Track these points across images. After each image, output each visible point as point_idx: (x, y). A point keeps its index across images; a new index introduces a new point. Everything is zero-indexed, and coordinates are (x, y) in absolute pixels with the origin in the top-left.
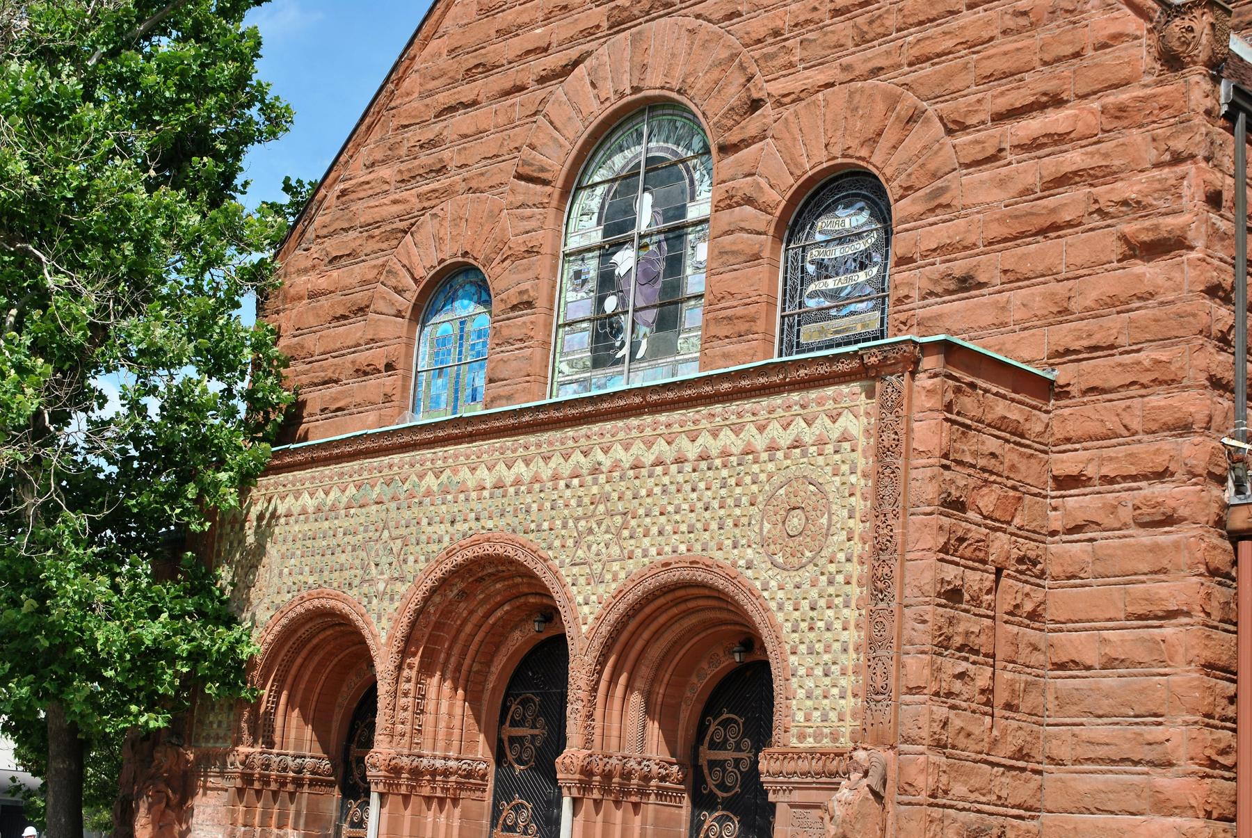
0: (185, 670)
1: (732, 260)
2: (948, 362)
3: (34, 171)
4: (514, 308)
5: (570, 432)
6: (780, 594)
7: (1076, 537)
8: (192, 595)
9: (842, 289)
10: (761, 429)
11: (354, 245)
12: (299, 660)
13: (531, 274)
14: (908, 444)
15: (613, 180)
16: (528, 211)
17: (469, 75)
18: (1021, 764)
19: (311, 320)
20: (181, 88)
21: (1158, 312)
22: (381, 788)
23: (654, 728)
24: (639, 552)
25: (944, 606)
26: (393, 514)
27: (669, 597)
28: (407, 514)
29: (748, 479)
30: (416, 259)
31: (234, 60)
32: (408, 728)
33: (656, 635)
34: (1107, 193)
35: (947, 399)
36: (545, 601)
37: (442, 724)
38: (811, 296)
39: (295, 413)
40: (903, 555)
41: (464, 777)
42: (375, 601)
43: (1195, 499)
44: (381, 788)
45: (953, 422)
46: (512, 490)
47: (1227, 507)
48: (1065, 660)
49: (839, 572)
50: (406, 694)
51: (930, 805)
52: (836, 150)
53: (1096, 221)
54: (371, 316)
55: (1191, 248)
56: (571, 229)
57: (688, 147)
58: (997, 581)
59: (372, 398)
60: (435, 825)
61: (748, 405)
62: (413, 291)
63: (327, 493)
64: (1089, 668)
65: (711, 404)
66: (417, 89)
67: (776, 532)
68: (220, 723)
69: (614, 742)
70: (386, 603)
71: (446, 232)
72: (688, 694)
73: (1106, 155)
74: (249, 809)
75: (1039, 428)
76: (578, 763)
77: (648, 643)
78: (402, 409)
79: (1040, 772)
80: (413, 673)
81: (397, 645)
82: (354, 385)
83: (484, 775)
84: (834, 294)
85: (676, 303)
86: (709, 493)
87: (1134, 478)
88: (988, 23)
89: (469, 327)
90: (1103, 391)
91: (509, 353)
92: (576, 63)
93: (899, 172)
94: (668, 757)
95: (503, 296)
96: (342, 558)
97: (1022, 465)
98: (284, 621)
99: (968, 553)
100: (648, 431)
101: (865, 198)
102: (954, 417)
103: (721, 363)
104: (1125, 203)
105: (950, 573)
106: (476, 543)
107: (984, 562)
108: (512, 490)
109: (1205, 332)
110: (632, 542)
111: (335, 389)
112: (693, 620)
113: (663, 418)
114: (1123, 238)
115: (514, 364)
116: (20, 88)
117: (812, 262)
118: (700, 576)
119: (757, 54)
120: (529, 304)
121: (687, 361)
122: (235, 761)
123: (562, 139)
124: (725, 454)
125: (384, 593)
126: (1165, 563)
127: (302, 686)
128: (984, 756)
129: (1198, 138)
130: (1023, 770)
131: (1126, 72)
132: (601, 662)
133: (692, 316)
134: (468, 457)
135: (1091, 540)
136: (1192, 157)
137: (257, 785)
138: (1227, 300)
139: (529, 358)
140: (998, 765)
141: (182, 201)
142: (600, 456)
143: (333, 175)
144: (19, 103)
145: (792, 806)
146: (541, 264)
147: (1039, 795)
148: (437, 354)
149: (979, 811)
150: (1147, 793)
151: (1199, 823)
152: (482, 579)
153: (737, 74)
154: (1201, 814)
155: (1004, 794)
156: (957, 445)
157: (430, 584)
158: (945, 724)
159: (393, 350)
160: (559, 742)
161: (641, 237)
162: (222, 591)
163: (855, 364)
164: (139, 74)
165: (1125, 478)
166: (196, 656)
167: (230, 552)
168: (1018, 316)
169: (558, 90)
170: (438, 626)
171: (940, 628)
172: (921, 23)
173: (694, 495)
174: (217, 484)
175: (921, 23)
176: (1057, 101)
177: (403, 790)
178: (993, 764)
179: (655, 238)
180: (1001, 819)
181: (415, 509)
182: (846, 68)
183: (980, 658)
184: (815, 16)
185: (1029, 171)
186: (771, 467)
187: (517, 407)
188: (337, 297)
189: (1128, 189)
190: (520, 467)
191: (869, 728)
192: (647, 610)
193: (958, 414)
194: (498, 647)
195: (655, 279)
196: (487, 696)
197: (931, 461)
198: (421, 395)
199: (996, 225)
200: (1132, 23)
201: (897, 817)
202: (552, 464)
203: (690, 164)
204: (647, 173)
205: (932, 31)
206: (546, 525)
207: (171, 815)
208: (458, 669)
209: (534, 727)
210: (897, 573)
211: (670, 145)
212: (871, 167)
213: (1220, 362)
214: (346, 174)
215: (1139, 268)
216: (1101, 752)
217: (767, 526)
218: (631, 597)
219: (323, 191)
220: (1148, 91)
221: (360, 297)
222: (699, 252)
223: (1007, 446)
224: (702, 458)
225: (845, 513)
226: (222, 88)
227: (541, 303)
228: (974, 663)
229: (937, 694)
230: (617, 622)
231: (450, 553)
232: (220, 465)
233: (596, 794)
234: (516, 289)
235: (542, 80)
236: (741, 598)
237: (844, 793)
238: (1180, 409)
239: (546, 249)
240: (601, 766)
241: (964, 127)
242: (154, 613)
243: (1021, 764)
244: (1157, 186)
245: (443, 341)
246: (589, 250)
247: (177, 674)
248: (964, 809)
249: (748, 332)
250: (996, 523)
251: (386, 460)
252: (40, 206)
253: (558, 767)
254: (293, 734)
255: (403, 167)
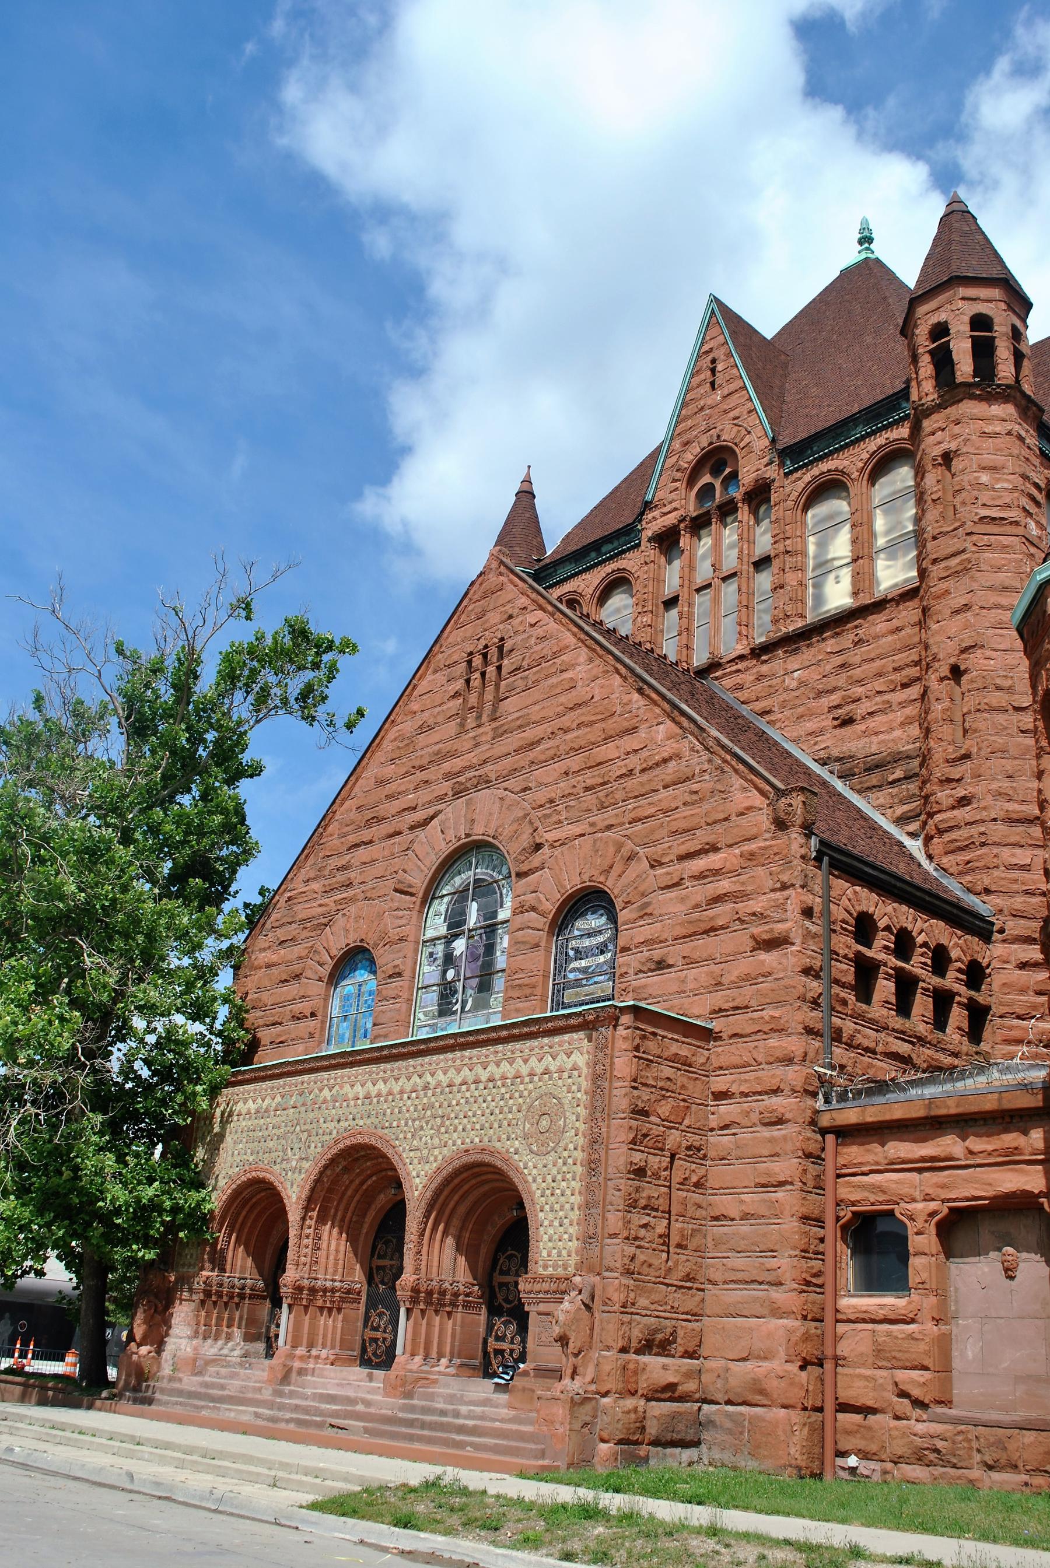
0: (168, 1219)
1: (522, 947)
2: (636, 1019)
3: (81, 890)
4: (390, 977)
5: (411, 1062)
6: (535, 1171)
7: (725, 1132)
8: (175, 1168)
9: (590, 967)
10: (526, 1061)
11: (294, 933)
12: (244, 1213)
13: (401, 954)
14: (611, 1073)
15: (454, 893)
16: (401, 913)
17: (368, 824)
18: (688, 1284)
19: (266, 983)
20: (187, 833)
21: (773, 985)
22: (289, 1300)
23: (461, 1260)
24: (450, 1142)
25: (633, 1179)
26: (303, 1115)
27: (470, 1172)
28: (311, 1115)
29: (517, 1095)
30: (331, 943)
31: (221, 814)
32: (308, 1260)
33: (462, 1198)
34: (746, 907)
35: (635, 1043)
36: (390, 1173)
37: (332, 1257)
38: (573, 970)
39: (254, 1045)
40: (607, 1146)
41: (346, 1293)
42: (290, 1173)
43: (795, 1107)
44: (289, 1300)
45: (640, 1058)
46: (375, 1100)
47: (818, 1112)
48: (718, 1214)
49: (570, 1157)
50: (308, 1237)
51: (622, 1313)
52: (586, 877)
53: (737, 926)
54: (304, 980)
55: (793, 944)
56: (428, 925)
57: (500, 873)
58: (672, 1162)
59: (302, 1035)
60: (326, 1326)
61: (518, 1046)
62: (329, 968)
63: (263, 1101)
64: (733, 1220)
65: (497, 1044)
66: (337, 832)
67: (533, 1130)
68: (192, 1255)
69: (435, 1270)
70: (296, 1175)
71: (351, 925)
72: (485, 1237)
73: (743, 884)
74: (208, 1314)
75: (702, 1060)
76: (410, 1285)
77: (457, 1203)
78: (320, 1042)
79: (703, 1290)
80: (313, 1223)
81: (302, 1203)
82: (290, 1025)
83: (360, 1292)
84: (584, 970)
85: (490, 974)
86: (493, 1104)
87: (760, 1093)
88: (675, 798)
89: (364, 988)
90: (741, 1036)
91: (387, 1006)
92: (432, 818)
93: (622, 892)
94: (471, 1280)
95: (384, 969)
96: (271, 1144)
97: (690, 1085)
98: (234, 1186)
99: (650, 1144)
100: (458, 1062)
101: (604, 907)
102: (640, 1055)
103: (515, 1015)
104: (754, 914)
105: (637, 1157)
106: (353, 1135)
107: (662, 1150)
108: (375, 1100)
109: (802, 998)
110: (447, 1135)
111: (279, 1028)
112: (486, 1187)
113: (467, 1053)
114: (753, 937)
115: (389, 1014)
116: (76, 837)
117: (572, 949)
118: (487, 1159)
119: (540, 814)
120: (399, 974)
121: (495, 1013)
122: (198, 1284)
123: (422, 866)
124: (504, 1078)
125: (296, 1168)
126: (778, 1150)
127: (246, 1230)
128: (662, 1280)
129: (796, 873)
130: (690, 1288)
131: (754, 831)
132: (427, 1216)
133: (499, 983)
134: (349, 1078)
135: (734, 1134)
136: (793, 885)
137: (214, 1298)
138: (817, 977)
139: (399, 1010)
140: (672, 1285)
141: (178, 907)
142: (429, 1078)
143: (283, 887)
144: (74, 846)
145: (539, 1314)
146: (408, 947)
147: (701, 1305)
148: (344, 1006)
149: (657, 1317)
150: (767, 1303)
151: (798, 1323)
152: (357, 1159)
153: (528, 826)
154: (800, 1317)
155: (676, 1305)
156: (643, 1073)
157: (323, 1162)
158: (633, 1258)
159: (315, 1003)
160: (400, 1271)
161: (470, 931)
162: (196, 1166)
163: (581, 1019)
164: (160, 824)
165: (754, 1093)
166: (176, 1210)
167: (204, 1137)
168: (692, 986)
169: (421, 834)
170: (330, 1190)
171: (630, 1194)
172: (636, 797)
173: (484, 1105)
174: (195, 1094)
175: (636, 797)
176: (714, 849)
177: (304, 1302)
178: (668, 1285)
179: (478, 932)
180: (674, 1322)
181: (316, 1112)
182: (592, 825)
183: (659, 1214)
184: (574, 791)
185: (698, 892)
186: (531, 1086)
187: (379, 1045)
188: (283, 967)
189: (756, 905)
190: (381, 1085)
191: (585, 1261)
192: (456, 1181)
193: (644, 1052)
194: (370, 1204)
195: (478, 958)
196: (362, 1238)
197: (625, 1084)
198: (333, 1033)
199: (678, 927)
200: (758, 801)
201: (601, 1321)
202: (400, 1083)
203: (500, 883)
204: (474, 889)
205: (643, 802)
206: (395, 1124)
207: (158, 1318)
208: (343, 1220)
209: (392, 1259)
210: (603, 1158)
211: (489, 871)
212: (606, 889)
213: (813, 1017)
214: (291, 886)
215: (763, 956)
216: (740, 1276)
217: (527, 1126)
218: (445, 1173)
219: (277, 897)
220: (768, 843)
221: (297, 968)
222: (504, 942)
223: (679, 1073)
224: (490, 1080)
225: (574, 1118)
226: (213, 832)
227: (407, 974)
228: (654, 1217)
229: (627, 1238)
230: (437, 1189)
231: (337, 1142)
232: (198, 1081)
233: (422, 1306)
234: (393, 964)
235: (412, 828)
236: (511, 1173)
237: (566, 1305)
238: (786, 1048)
239: (411, 938)
240: (425, 1285)
241: (661, 864)
242: (150, 1181)
243: (688, 1284)
244: (773, 904)
245: (346, 998)
246: (438, 939)
247: (163, 1223)
248: (646, 1315)
249: (531, 995)
250: (671, 1123)
251: (300, 1078)
252: (86, 910)
253: (398, 1287)
254: (239, 1264)
255: (327, 882)
